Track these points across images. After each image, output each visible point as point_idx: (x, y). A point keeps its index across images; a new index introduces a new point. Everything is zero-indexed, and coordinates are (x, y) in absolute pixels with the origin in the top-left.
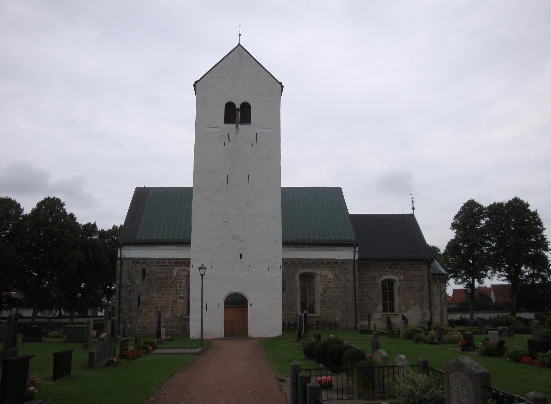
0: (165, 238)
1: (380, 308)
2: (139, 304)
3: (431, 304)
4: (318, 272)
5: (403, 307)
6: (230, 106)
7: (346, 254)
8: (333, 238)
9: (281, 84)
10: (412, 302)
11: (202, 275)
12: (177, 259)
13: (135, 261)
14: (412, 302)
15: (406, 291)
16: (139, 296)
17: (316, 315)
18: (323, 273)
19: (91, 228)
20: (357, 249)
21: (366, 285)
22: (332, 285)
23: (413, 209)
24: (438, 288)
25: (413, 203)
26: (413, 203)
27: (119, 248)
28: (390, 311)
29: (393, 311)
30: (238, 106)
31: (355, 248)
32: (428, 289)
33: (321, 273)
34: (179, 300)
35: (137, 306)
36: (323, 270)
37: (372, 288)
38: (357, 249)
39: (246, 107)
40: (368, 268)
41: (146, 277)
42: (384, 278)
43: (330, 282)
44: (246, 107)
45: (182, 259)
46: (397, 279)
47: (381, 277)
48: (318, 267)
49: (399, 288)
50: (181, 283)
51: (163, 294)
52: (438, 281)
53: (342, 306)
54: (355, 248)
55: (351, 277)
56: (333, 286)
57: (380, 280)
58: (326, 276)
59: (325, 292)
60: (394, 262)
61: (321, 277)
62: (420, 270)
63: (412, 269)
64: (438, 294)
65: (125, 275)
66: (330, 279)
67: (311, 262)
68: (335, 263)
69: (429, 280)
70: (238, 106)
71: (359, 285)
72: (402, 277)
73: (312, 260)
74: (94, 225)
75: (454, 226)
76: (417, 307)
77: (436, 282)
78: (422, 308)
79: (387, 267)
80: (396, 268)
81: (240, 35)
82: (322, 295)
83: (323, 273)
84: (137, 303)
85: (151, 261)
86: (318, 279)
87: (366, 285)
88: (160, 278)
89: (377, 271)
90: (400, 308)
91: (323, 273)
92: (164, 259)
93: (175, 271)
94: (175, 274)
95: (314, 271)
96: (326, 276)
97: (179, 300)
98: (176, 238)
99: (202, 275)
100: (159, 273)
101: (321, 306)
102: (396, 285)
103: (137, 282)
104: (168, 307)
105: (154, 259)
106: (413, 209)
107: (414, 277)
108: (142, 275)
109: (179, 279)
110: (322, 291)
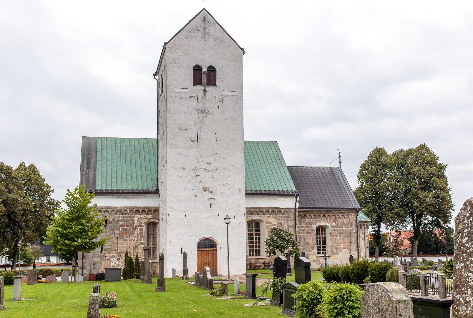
1: (315, 251)
2: (102, 250)
3: (358, 247)
4: (264, 220)
5: (334, 250)
6: (197, 69)
7: (289, 203)
8: (263, 189)
9: (242, 49)
10: (342, 246)
11: (227, 224)
12: (137, 207)
13: (100, 210)
14: (342, 246)
15: (337, 236)
18: (268, 221)
20: (298, 199)
21: (303, 230)
23: (340, 162)
25: (340, 157)
26: (340, 157)
28: (256, 255)
29: (259, 254)
30: (205, 70)
31: (296, 198)
32: (356, 235)
34: (140, 246)
35: (100, 252)
36: (268, 217)
37: (309, 233)
38: (298, 199)
39: (212, 70)
40: (305, 215)
41: (108, 225)
42: (319, 224)
44: (212, 70)
45: (143, 207)
46: (329, 225)
47: (316, 224)
48: (264, 214)
49: (331, 233)
50: (141, 230)
51: (125, 240)
52: (363, 227)
54: (296, 198)
55: (292, 223)
57: (315, 226)
58: (271, 223)
60: (328, 211)
61: (267, 223)
62: (349, 218)
63: (342, 217)
67: (258, 210)
68: (279, 211)
69: (357, 226)
70: (205, 70)
71: (299, 230)
72: (334, 223)
73: (259, 208)
76: (347, 250)
77: (361, 228)
78: (350, 251)
79: (321, 215)
80: (329, 216)
83: (269, 220)
85: (113, 209)
86: (263, 226)
87: (303, 230)
88: (121, 226)
89: (312, 218)
90: (332, 251)
92: (125, 207)
93: (136, 219)
94: (136, 222)
95: (260, 218)
96: (271, 223)
97: (140, 246)
98: (109, 188)
99: (227, 224)
100: (120, 221)
102: (328, 231)
105: (116, 207)
106: (340, 162)
107: (344, 224)
109: (140, 226)
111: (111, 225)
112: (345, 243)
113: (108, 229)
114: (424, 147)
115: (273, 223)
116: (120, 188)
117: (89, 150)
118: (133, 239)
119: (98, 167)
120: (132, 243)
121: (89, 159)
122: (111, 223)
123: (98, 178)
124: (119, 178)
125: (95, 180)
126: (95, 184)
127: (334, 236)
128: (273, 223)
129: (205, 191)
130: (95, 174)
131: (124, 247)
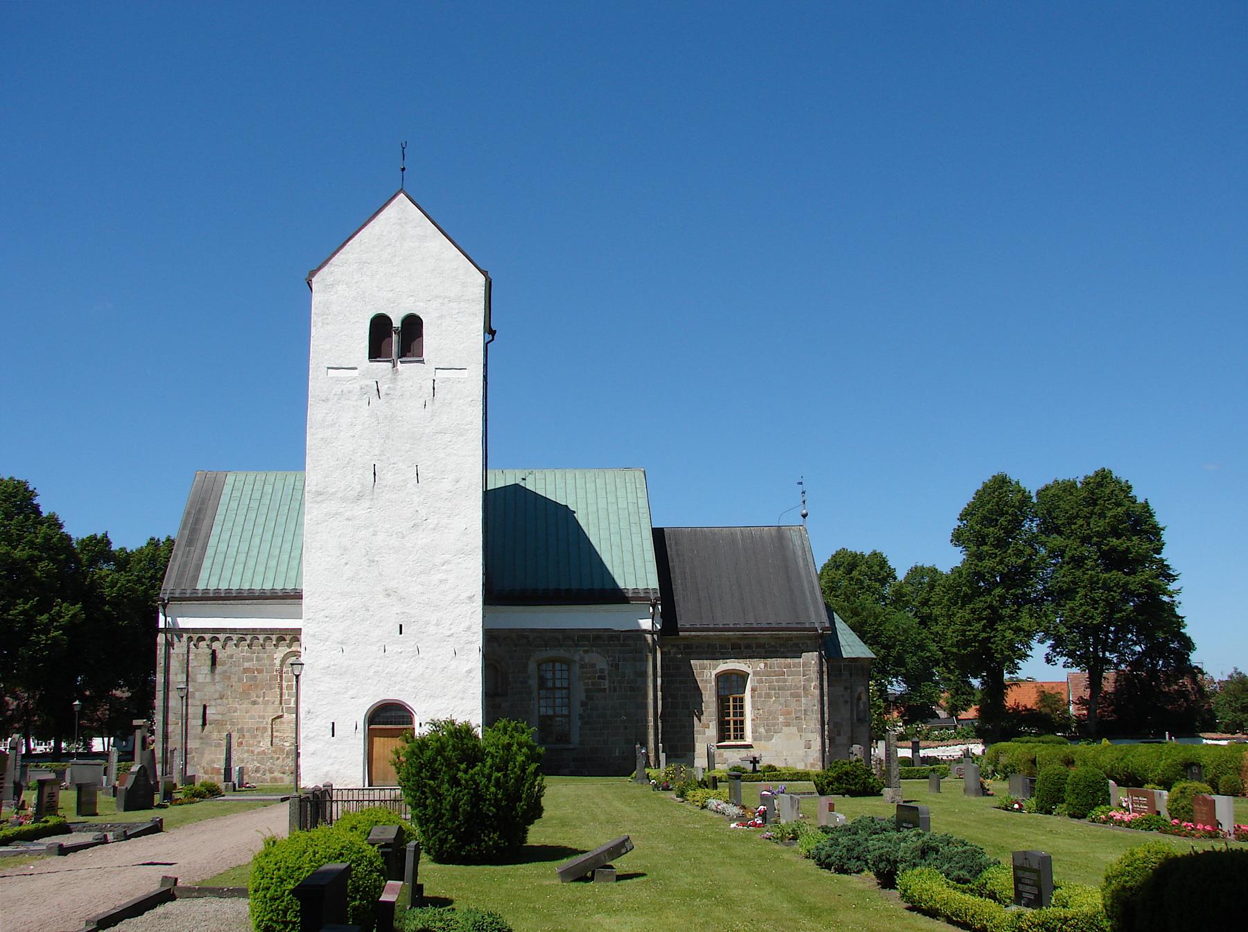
0: (257, 586)
2: (204, 724)
4: (577, 658)
5: (762, 730)
6: (380, 326)
11: (297, 676)
14: (781, 719)
15: (768, 696)
16: (205, 707)
17: (571, 746)
18: (587, 660)
19: (99, 547)
22: (606, 684)
24: (846, 689)
27: (161, 609)
28: (736, 738)
29: (742, 738)
30: (397, 323)
33: (582, 659)
36: (585, 652)
41: (219, 668)
43: (600, 678)
44: (413, 325)
46: (749, 671)
48: (577, 645)
51: (254, 703)
53: (626, 728)
56: (607, 686)
57: (714, 673)
58: (593, 666)
59: (590, 698)
61: (582, 666)
64: (846, 702)
65: (175, 664)
66: (602, 671)
70: (397, 323)
74: (105, 541)
75: (958, 538)
76: (794, 730)
81: (403, 169)
82: (583, 704)
84: (200, 722)
88: (246, 670)
91: (587, 660)
94: (278, 662)
96: (593, 666)
101: (580, 728)
103: (200, 678)
104: (265, 729)
108: (209, 663)
110: (583, 696)
111: (225, 668)
112: (789, 713)
113: (217, 678)
114: (1103, 477)
115: (598, 667)
116: (246, 587)
117: (203, 502)
118: (272, 699)
119: (213, 541)
120: (270, 709)
121: (197, 521)
122: (223, 664)
123: (207, 563)
124: (251, 563)
125: (198, 568)
126: (196, 578)
127: (760, 696)
128: (598, 667)
129: (389, 595)
130: (201, 559)
131: (252, 717)
